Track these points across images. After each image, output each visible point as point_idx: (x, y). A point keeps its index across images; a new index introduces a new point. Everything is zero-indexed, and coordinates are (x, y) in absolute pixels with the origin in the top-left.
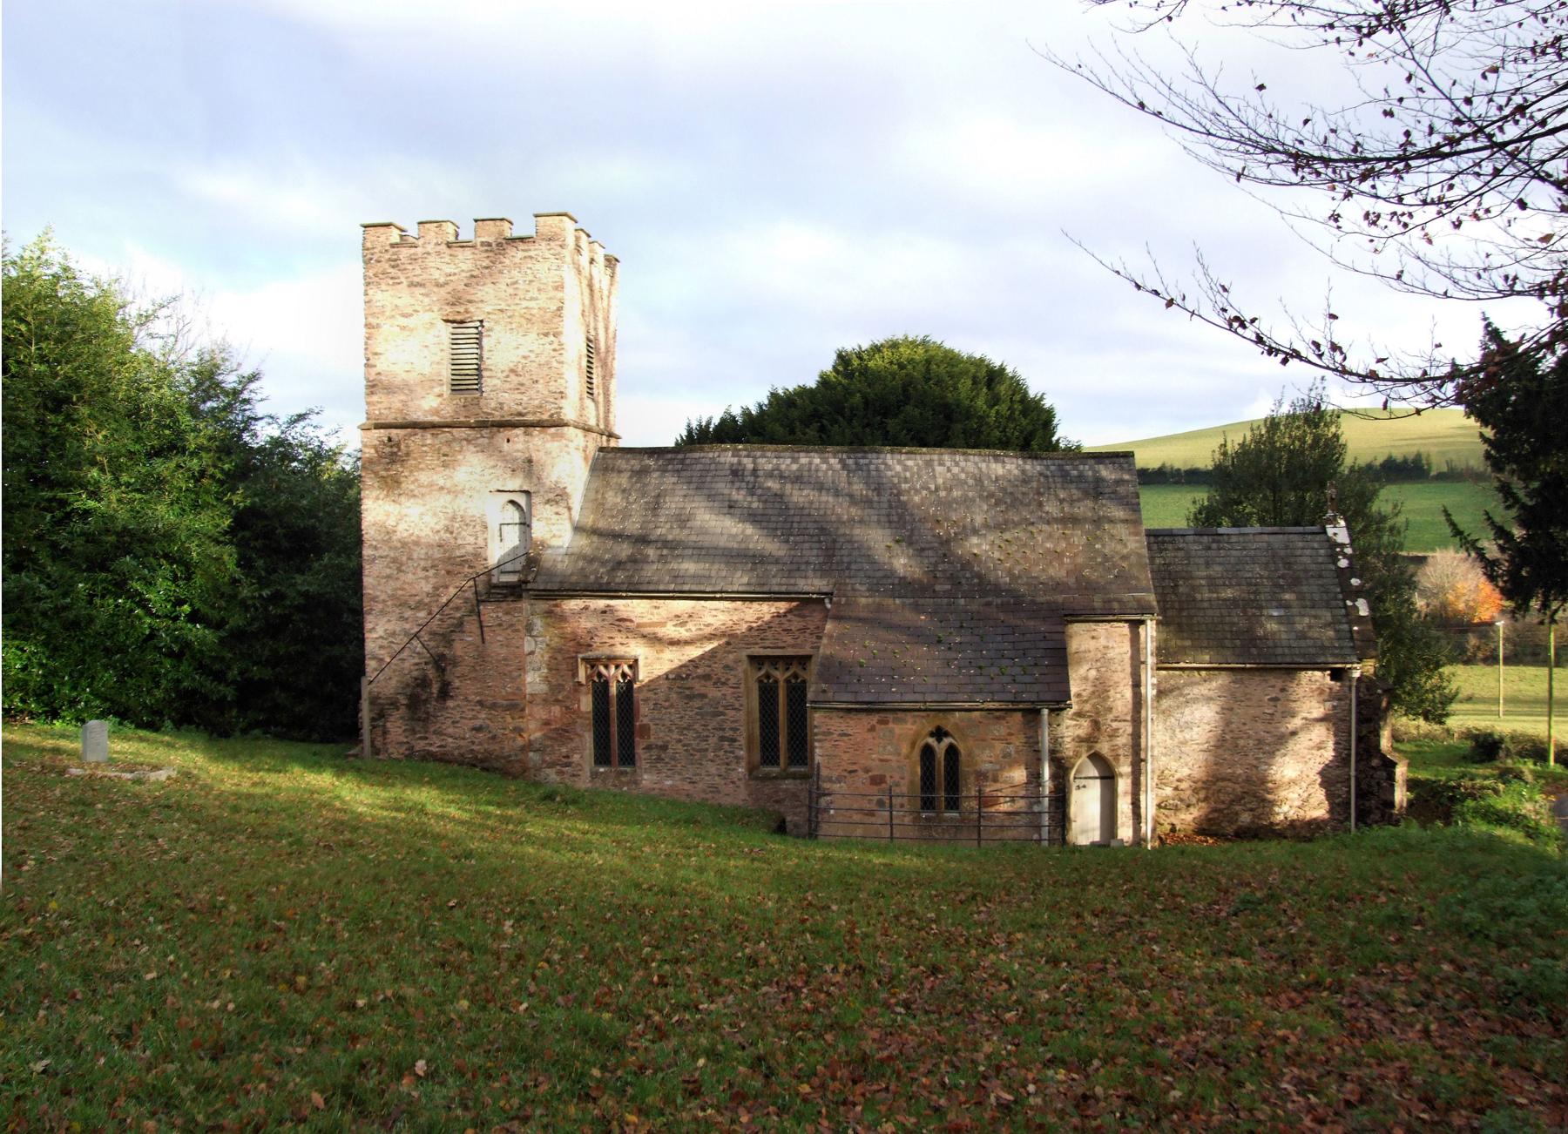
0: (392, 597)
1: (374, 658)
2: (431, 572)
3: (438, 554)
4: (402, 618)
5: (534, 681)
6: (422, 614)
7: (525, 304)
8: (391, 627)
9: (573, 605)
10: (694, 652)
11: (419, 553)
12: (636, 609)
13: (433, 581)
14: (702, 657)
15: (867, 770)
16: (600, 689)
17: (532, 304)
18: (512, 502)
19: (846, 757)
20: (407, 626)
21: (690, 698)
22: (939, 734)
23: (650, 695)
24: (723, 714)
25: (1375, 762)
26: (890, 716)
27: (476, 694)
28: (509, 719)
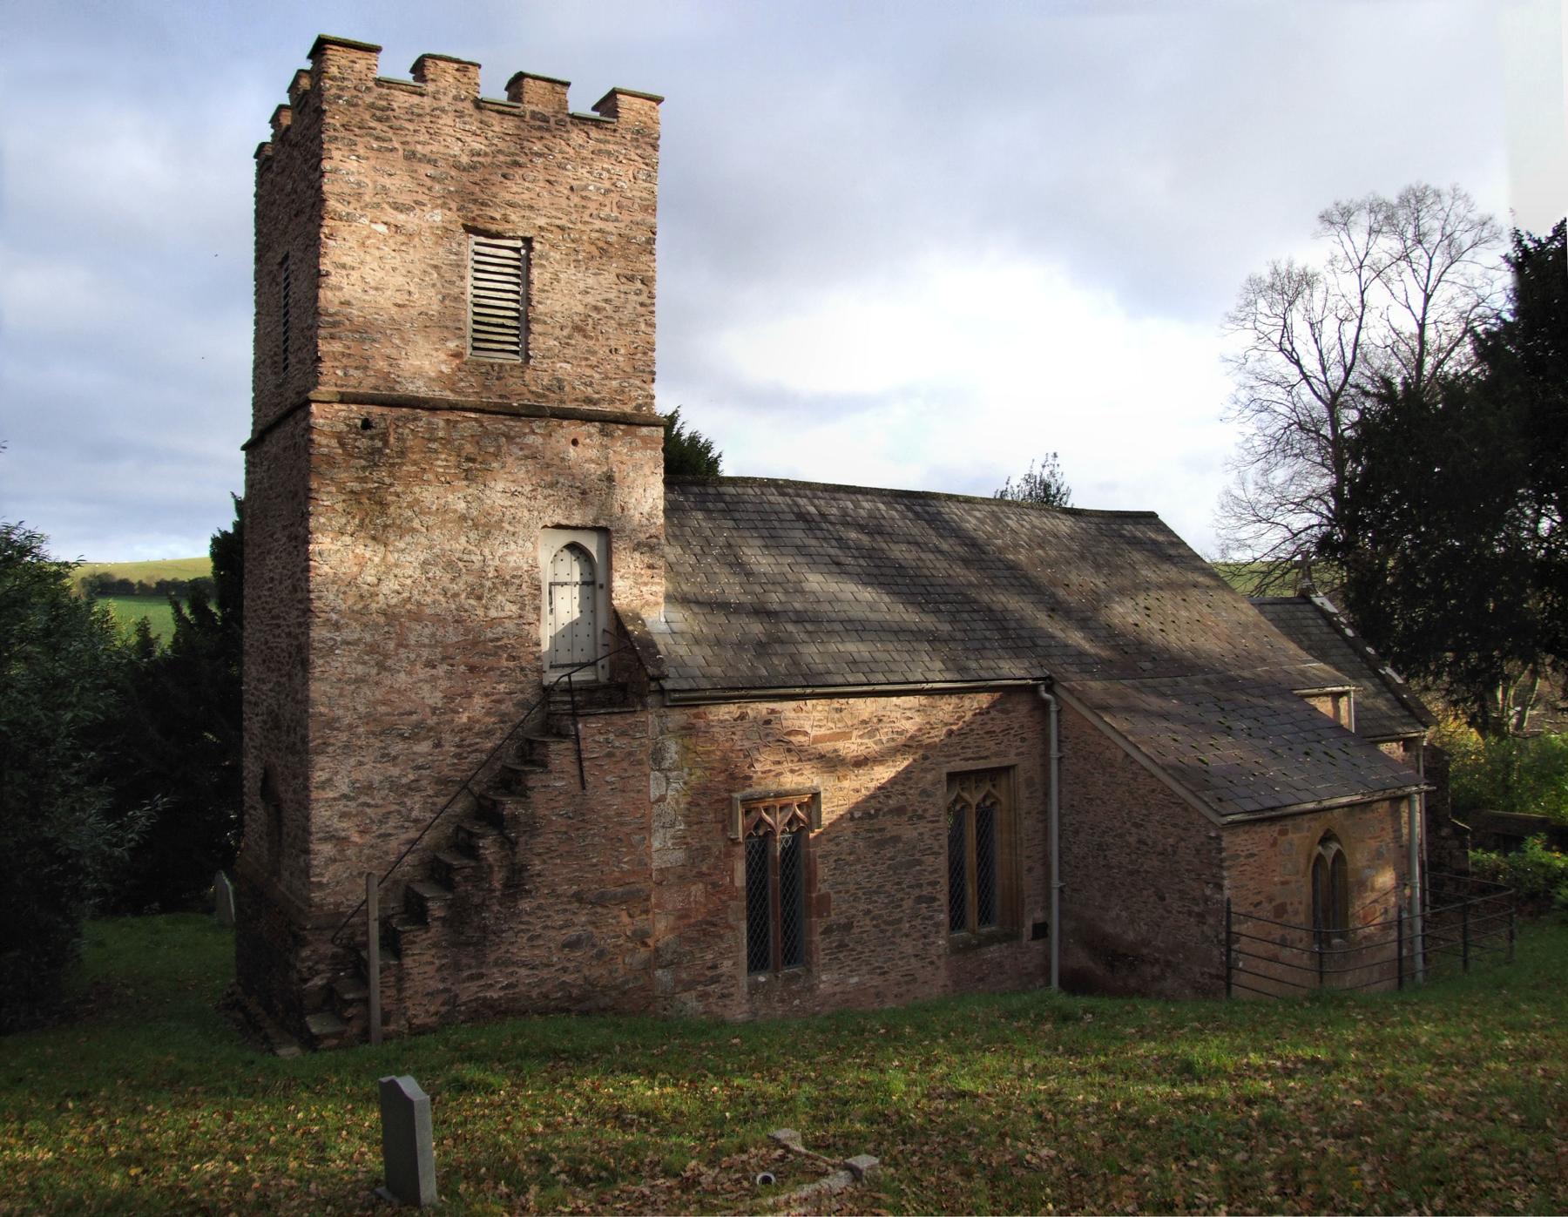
0: (369, 718)
1: (330, 837)
2: (442, 670)
3: (452, 636)
4: (386, 757)
5: (663, 850)
6: (424, 747)
7: (598, 224)
8: (361, 775)
9: (726, 712)
10: (883, 774)
11: (419, 633)
12: (810, 719)
13: (444, 684)
14: (893, 781)
15: (1270, 900)
16: (760, 842)
17: (609, 227)
18: (573, 547)
19: (1251, 885)
20: (395, 772)
21: (881, 844)
22: (1327, 838)
23: (831, 847)
24: (919, 862)
25: (1445, 832)
26: (1289, 823)
27: (571, 881)
28: (625, 919)
